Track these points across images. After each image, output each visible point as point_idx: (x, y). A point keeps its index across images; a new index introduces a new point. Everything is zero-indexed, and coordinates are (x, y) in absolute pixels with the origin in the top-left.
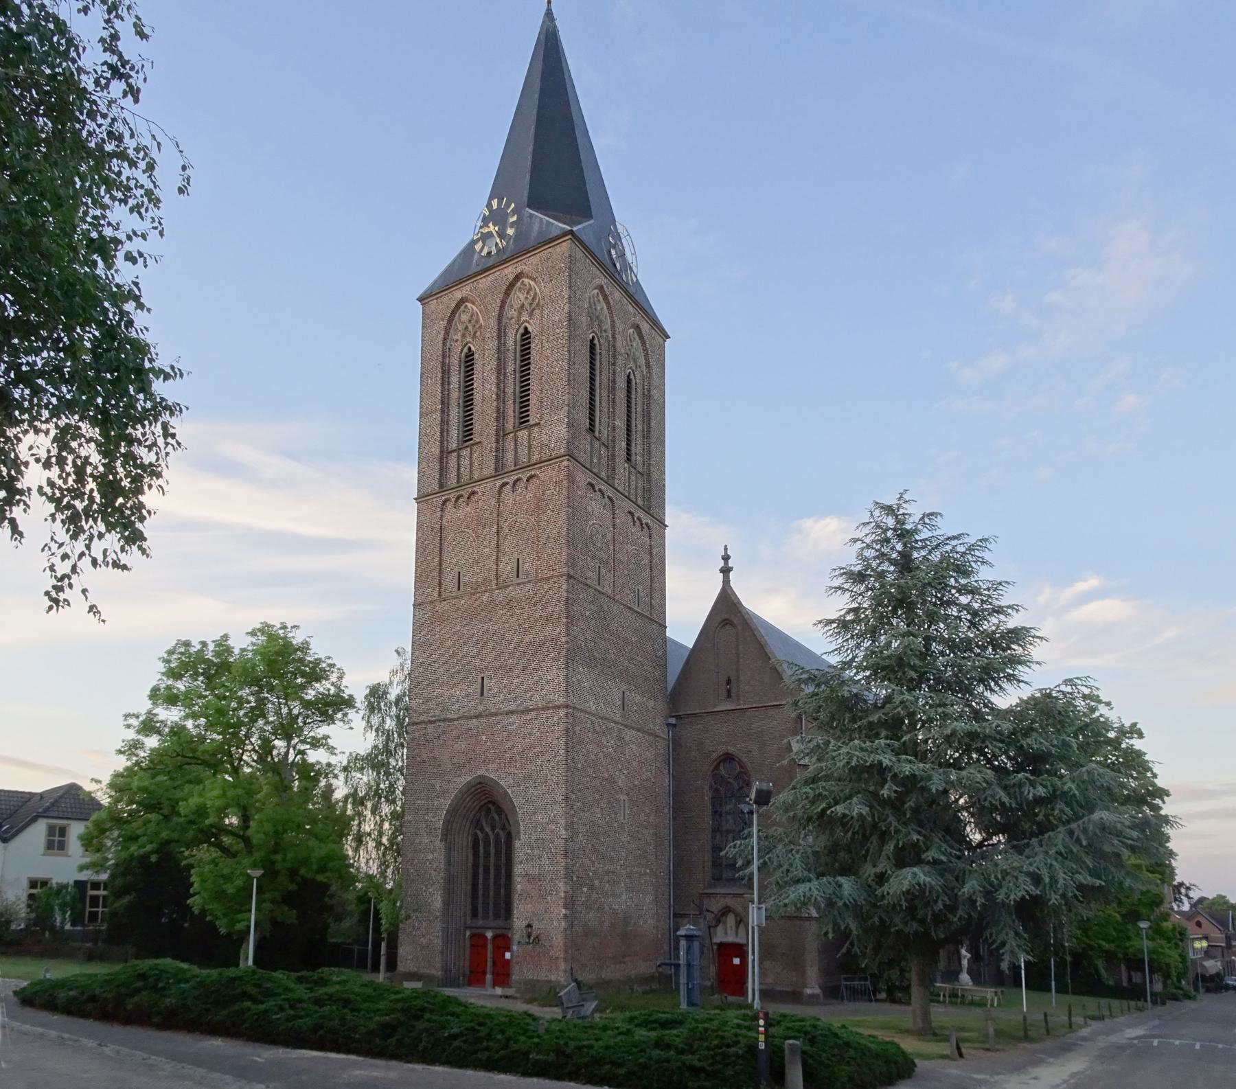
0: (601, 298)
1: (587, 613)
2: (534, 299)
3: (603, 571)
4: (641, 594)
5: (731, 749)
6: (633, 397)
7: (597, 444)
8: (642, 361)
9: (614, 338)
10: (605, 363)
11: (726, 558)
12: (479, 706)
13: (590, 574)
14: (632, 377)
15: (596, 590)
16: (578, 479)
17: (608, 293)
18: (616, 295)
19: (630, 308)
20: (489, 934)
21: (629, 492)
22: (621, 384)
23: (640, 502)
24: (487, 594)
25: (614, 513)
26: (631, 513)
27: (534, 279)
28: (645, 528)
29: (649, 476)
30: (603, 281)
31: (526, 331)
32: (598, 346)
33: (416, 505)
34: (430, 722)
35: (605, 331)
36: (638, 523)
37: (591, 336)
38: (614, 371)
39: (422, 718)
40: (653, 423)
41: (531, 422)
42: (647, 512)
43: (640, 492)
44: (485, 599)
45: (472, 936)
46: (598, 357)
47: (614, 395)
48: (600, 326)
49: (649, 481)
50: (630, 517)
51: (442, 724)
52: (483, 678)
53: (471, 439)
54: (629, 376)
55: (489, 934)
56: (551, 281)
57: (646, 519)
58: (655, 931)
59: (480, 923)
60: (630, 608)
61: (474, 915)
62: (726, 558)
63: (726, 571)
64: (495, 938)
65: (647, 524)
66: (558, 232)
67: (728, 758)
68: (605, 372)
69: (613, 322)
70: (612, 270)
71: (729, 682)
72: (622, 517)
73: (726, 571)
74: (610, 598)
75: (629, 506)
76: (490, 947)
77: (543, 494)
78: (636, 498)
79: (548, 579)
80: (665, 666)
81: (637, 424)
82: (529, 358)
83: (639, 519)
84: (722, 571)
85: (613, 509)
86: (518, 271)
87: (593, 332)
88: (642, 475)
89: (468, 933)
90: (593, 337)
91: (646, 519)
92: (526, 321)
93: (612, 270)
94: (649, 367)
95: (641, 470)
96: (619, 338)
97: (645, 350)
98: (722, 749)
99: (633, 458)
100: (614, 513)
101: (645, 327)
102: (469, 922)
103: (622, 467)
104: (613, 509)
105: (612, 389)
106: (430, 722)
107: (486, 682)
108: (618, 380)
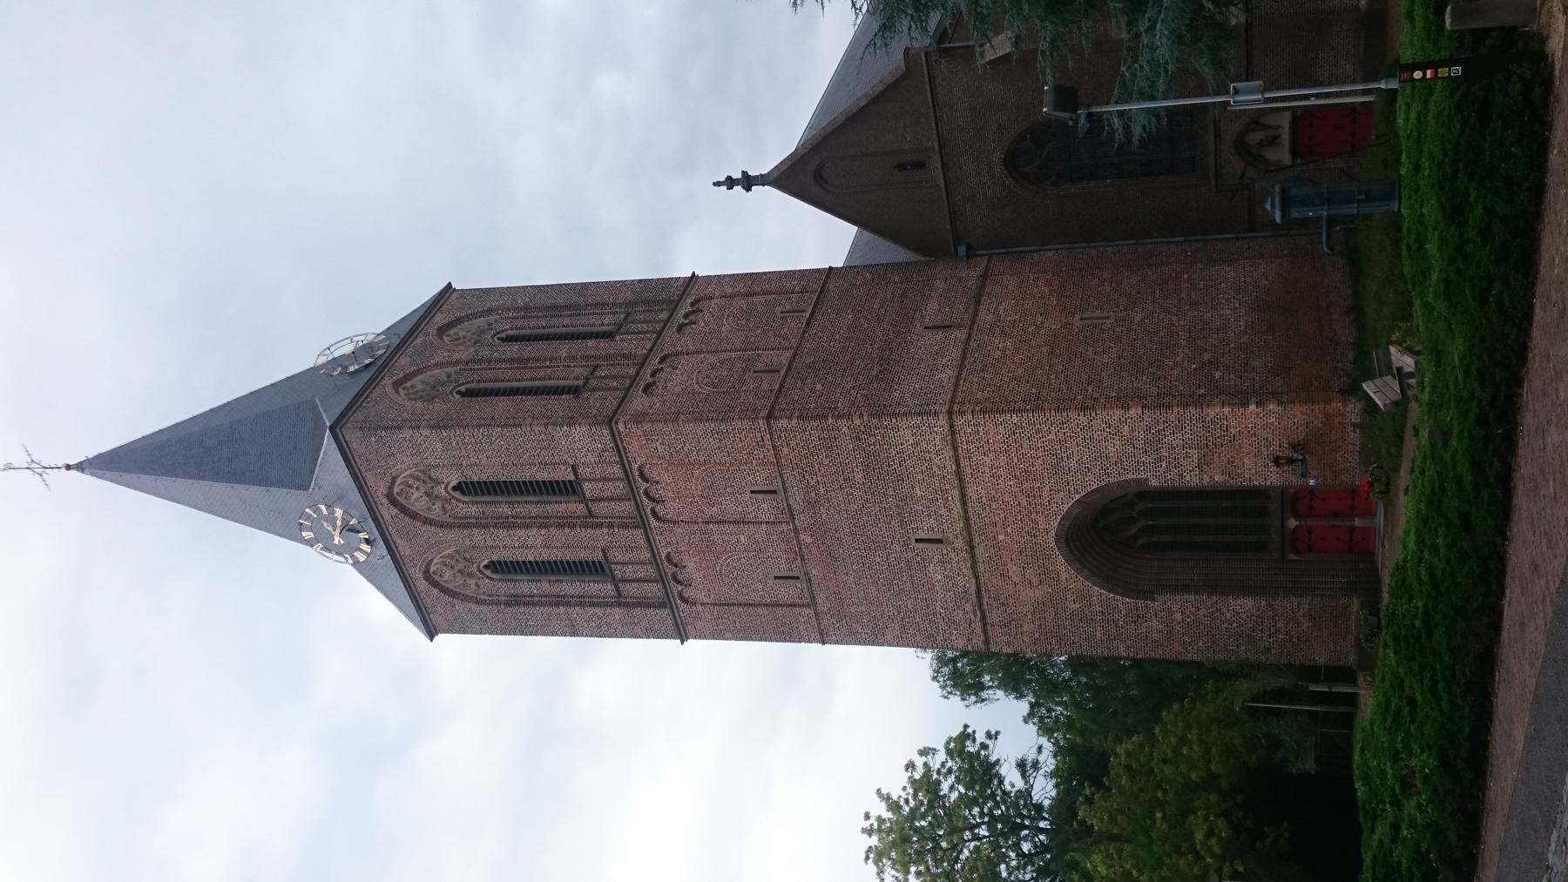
0: (408, 384)
1: (819, 387)
2: (417, 478)
3: (760, 366)
4: (788, 307)
5: (998, 157)
6: (528, 332)
7: (594, 382)
8: (481, 322)
9: (457, 363)
10: (490, 375)
11: (730, 183)
12: (956, 545)
13: (765, 386)
14: (503, 335)
15: (786, 376)
16: (640, 408)
17: (401, 375)
18: (404, 363)
19: (418, 341)
20: (1293, 523)
21: (651, 332)
22: (514, 349)
23: (664, 315)
24: (802, 537)
25: (681, 353)
26: (680, 328)
27: (394, 479)
28: (700, 305)
29: (629, 304)
30: (388, 382)
32: (469, 386)
33: (690, 641)
34: (983, 618)
35: (449, 376)
36: (692, 317)
37: (457, 397)
38: (499, 361)
39: (979, 631)
40: (560, 301)
41: (572, 477)
42: (674, 305)
43: (650, 317)
44: (809, 540)
45: (1296, 551)
46: (482, 385)
47: (528, 360)
48: (443, 384)
49: (636, 303)
50: (687, 330)
51: (985, 600)
52: (917, 541)
54: (503, 340)
55: (1293, 523)
56: (393, 455)
57: (686, 307)
60: (808, 323)
62: (730, 183)
63: (748, 182)
64: (1297, 516)
65: (693, 304)
67: (1012, 161)
68: (500, 374)
69: (437, 366)
70: (374, 369)
71: (901, 167)
72: (686, 342)
73: (748, 182)
74: (795, 355)
75: (670, 332)
76: (1311, 522)
77: (664, 458)
78: (658, 322)
79: (774, 447)
80: (886, 266)
81: (563, 324)
83: (686, 316)
84: (748, 189)
85: (677, 354)
86: (385, 501)
87: (451, 393)
88: (628, 314)
89: (1292, 556)
90: (458, 392)
91: (686, 307)
92: (446, 488)
93: (374, 369)
94: (490, 311)
95: (622, 316)
96: (456, 356)
97: (468, 317)
99: (607, 328)
100: (681, 353)
101: (440, 319)
103: (622, 344)
104: (677, 354)
105: (522, 361)
106: (983, 618)
107: (922, 535)
108: (508, 355)
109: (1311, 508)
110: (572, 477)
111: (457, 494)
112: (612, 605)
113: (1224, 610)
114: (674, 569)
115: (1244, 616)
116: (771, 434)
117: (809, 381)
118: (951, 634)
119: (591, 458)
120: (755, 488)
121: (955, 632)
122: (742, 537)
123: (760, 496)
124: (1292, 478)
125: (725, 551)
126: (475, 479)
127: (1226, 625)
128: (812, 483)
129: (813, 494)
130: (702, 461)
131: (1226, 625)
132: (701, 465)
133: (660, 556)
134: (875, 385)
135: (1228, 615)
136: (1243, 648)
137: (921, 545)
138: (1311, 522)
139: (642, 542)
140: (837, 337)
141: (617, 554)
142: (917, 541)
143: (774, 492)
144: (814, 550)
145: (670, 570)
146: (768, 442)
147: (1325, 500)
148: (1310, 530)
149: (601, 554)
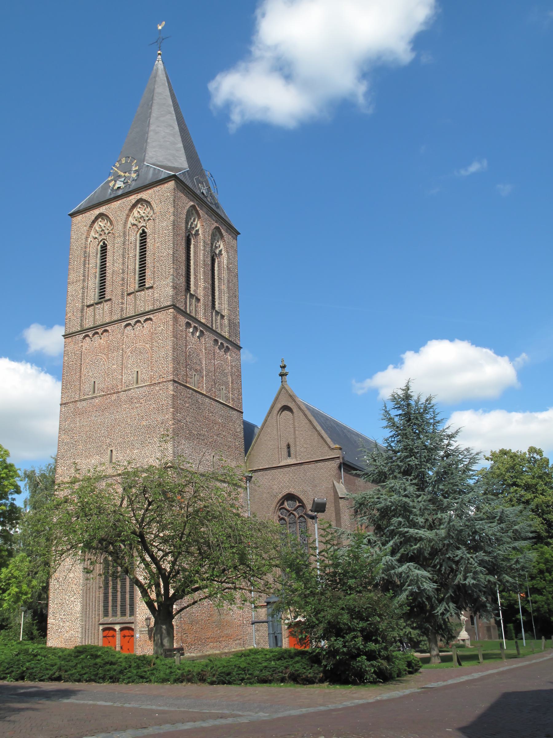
1: (187, 405)
5: (292, 491)
20: (117, 628)
31: (144, 232)
41: (147, 286)
44: (113, 398)
45: (104, 630)
52: (112, 451)
53: (104, 297)
55: (117, 628)
56: (161, 203)
58: (241, 619)
59: (110, 619)
61: (106, 614)
66: (166, 176)
67: (290, 497)
76: (118, 636)
77: (155, 330)
82: (146, 248)
89: (101, 627)
98: (285, 492)
102: (101, 621)
107: (114, 453)
109: (124, 636)
110: (147, 286)
111: (141, 231)
112: (83, 302)
113: (75, 597)
114: (100, 333)
115: (72, 606)
116: (166, 382)
117: (190, 400)
118: (64, 467)
119: (156, 295)
120: (139, 373)
121: (65, 469)
122: (116, 366)
123: (135, 375)
124: (140, 625)
125: (108, 358)
126: (148, 240)
127: (67, 598)
128: (141, 401)
129: (135, 401)
130: (153, 348)
131: (67, 598)
132: (151, 348)
133: (106, 327)
134: (188, 432)
135: (72, 599)
136: (56, 606)
137: (109, 452)
138: (118, 636)
139: (115, 318)
140: (211, 415)
141: (108, 306)
142: (112, 451)
143: (137, 382)
144: (109, 400)
145: (100, 331)
146: (161, 380)
147: (128, 642)
148: (114, 636)
149: (109, 298)
